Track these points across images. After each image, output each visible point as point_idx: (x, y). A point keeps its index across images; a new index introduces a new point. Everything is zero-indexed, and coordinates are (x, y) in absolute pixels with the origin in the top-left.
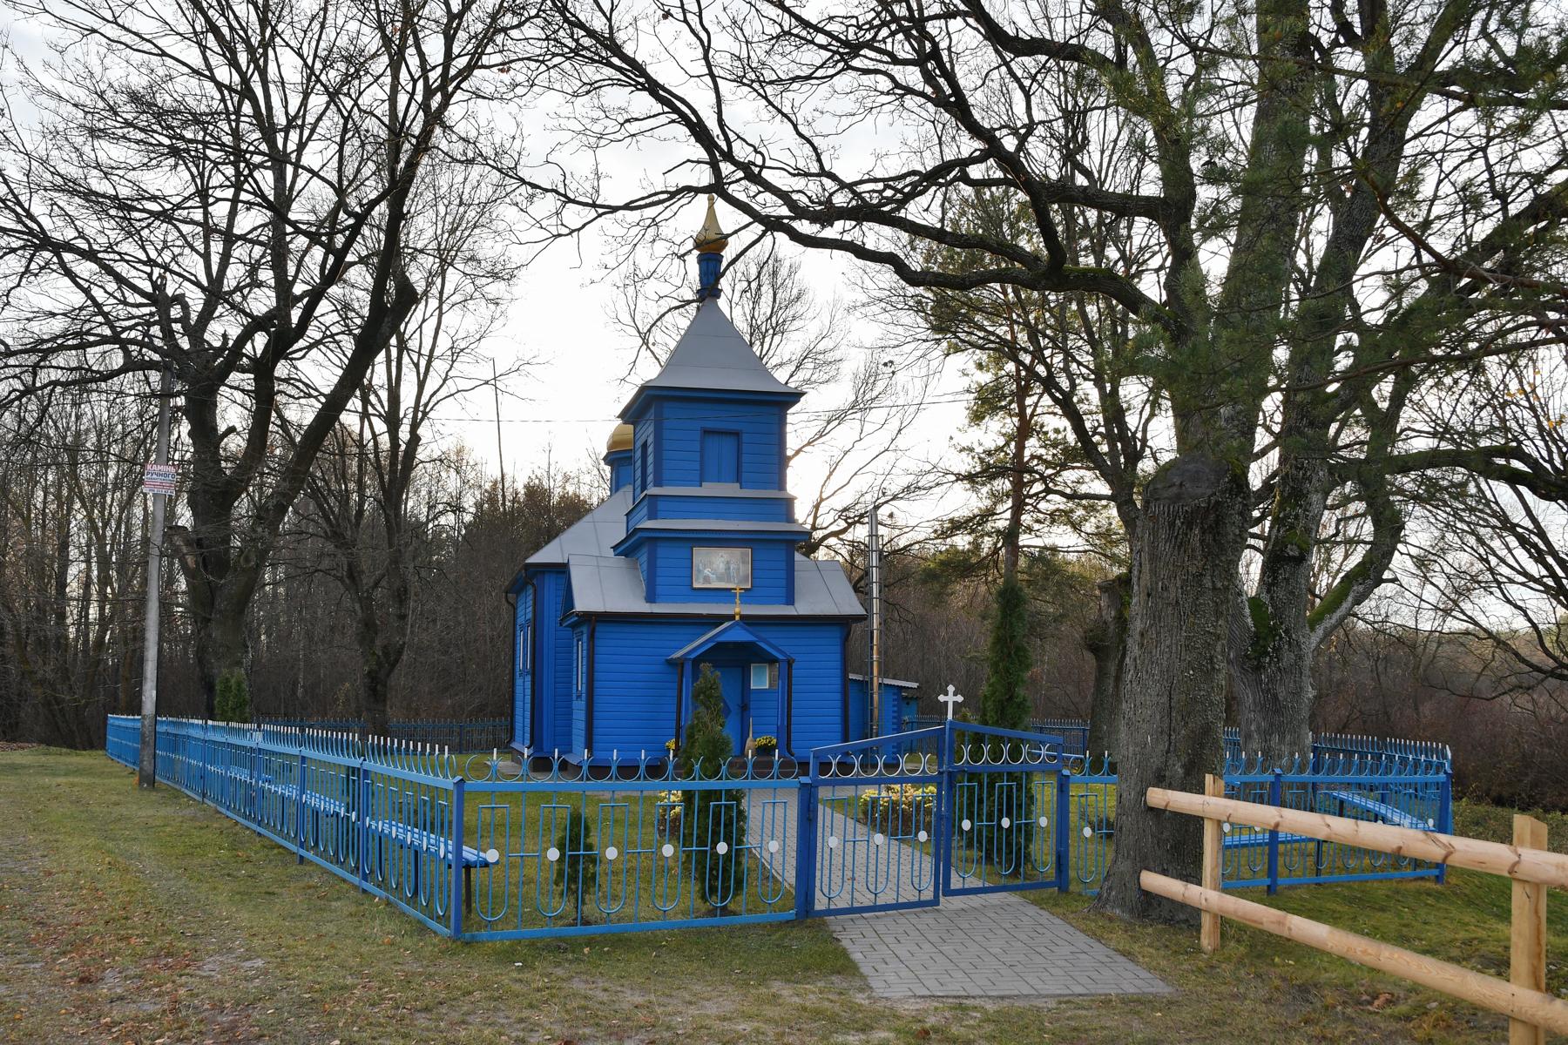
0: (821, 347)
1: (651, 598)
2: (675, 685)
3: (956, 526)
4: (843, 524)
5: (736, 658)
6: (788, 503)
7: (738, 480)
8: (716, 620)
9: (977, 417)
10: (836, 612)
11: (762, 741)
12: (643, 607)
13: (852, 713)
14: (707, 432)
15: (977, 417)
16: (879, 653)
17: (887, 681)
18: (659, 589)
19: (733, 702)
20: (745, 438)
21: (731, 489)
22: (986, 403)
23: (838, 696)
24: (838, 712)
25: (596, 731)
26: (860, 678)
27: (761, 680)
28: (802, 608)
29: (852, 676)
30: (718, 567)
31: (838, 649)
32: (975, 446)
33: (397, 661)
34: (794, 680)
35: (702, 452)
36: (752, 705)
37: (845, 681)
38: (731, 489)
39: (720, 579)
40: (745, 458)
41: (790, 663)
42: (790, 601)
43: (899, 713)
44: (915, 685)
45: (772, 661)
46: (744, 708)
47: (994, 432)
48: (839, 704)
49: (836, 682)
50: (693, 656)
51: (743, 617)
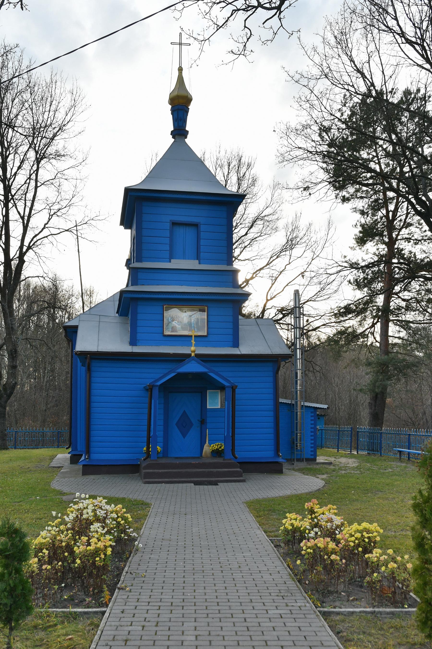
0: (266, 213)
1: (133, 343)
2: (147, 405)
3: (347, 310)
4: (281, 316)
5: (200, 384)
6: (235, 272)
7: (198, 258)
8: (182, 358)
9: (361, 241)
10: (270, 353)
11: (215, 446)
12: (126, 348)
13: (282, 424)
14: (174, 224)
15: (361, 241)
16: (301, 385)
17: (307, 404)
18: (139, 336)
19: (195, 418)
20: (202, 228)
21: (192, 264)
22: (367, 234)
23: (272, 414)
24: (272, 425)
25: (92, 439)
26: (289, 402)
27: (214, 402)
28: (244, 349)
29: (281, 400)
30: (182, 320)
31: (271, 379)
32: (360, 262)
33: (11, 393)
34: (237, 402)
35: (171, 238)
36: (209, 420)
37: (277, 405)
38: (192, 264)
39: (183, 329)
40: (202, 242)
41: (233, 389)
42: (236, 345)
43: (315, 424)
44: (325, 406)
45: (222, 388)
46: (203, 422)
47: (373, 250)
48: (272, 419)
49: (270, 403)
50: (159, 383)
51: (197, 355)
